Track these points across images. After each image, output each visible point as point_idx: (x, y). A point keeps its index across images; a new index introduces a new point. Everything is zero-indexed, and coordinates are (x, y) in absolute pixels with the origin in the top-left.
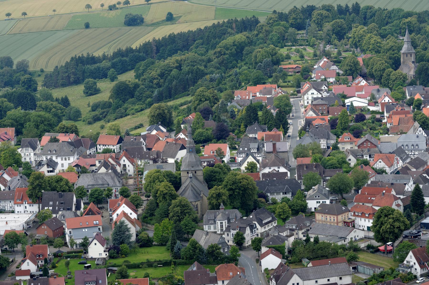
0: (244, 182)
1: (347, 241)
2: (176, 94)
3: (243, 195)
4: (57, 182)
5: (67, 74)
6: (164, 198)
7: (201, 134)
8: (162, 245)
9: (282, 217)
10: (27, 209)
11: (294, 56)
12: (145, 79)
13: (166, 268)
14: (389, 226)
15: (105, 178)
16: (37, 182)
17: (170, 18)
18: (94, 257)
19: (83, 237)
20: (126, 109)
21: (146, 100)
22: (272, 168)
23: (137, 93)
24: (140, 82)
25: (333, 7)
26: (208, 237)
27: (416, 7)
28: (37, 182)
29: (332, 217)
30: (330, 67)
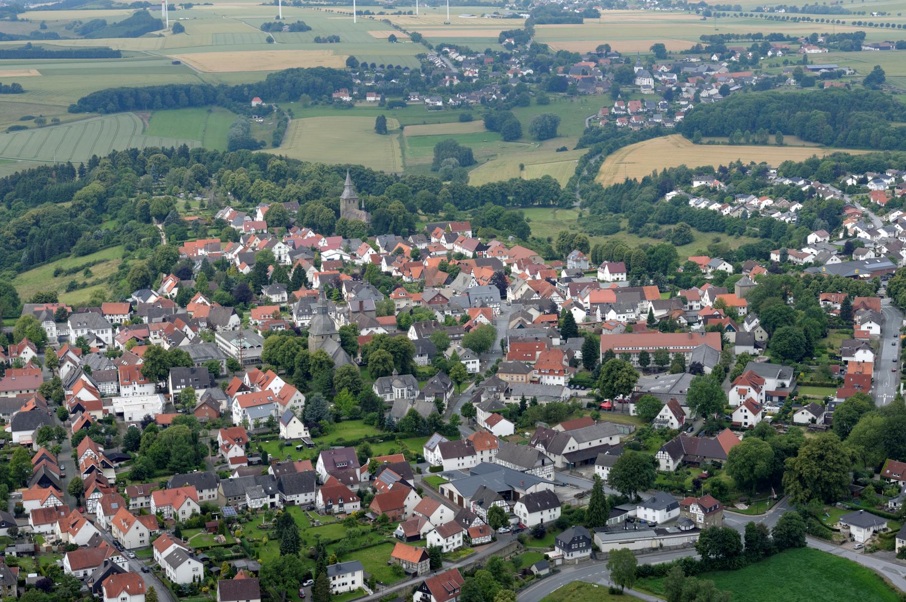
2: (51, 256)
4: (176, 355)
6: (321, 366)
8: (351, 419)
10: (137, 390)
14: (624, 380)
22: (370, 330)
29: (520, 377)
30: (243, 217)
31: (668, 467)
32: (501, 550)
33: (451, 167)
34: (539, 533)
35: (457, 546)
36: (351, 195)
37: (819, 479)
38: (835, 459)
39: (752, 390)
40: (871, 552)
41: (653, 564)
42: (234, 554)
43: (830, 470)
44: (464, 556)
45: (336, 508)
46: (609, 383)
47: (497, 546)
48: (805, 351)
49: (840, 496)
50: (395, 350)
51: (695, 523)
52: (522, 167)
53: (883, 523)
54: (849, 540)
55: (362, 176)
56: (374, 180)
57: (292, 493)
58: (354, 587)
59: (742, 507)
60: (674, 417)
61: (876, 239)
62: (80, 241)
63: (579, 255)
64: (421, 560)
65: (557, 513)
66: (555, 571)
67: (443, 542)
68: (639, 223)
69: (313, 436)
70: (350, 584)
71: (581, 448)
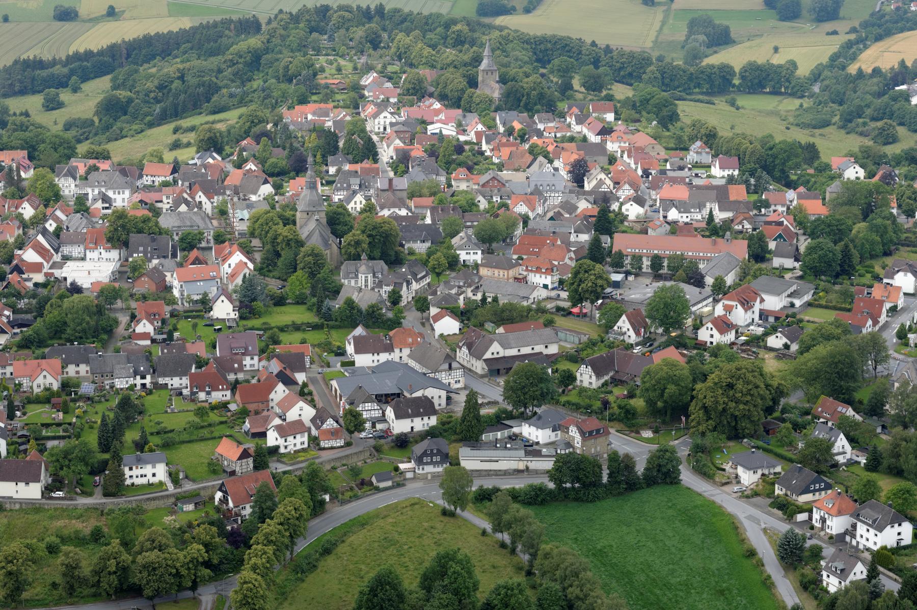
0: (386, 227)
1: (531, 301)
3: (384, 243)
4: (144, 222)
5: (10, 82)
6: (288, 244)
7: (275, 165)
8: (297, 303)
9: (437, 270)
10: (103, 256)
11: (330, 70)
12: (138, 92)
13: (316, 332)
14: (590, 284)
15: (194, 218)
16: (121, 222)
17: (112, 13)
18: (220, 317)
19: (203, 292)
20: (121, 130)
21: (144, 118)
22: (392, 210)
23: (131, 110)
24: (134, 96)
25: (352, 8)
26: (361, 294)
27: (423, 6)
28: (121, 222)
29: (501, 272)
30: (383, 84)
31: (591, 383)
32: (347, 456)
33: (698, 45)
34: (403, 442)
35: (299, 447)
36: (489, 65)
37: (724, 410)
38: (744, 390)
39: (739, 306)
40: (747, 497)
41: (517, 487)
42: (61, 434)
43: (737, 402)
44: (303, 459)
45: (202, 396)
46: (575, 286)
47: (349, 451)
48: (839, 268)
49: (747, 431)
50: (374, 233)
51: (573, 447)
52: (776, 50)
53: (774, 467)
54: (734, 481)
55: (567, 48)
56: (580, 53)
57: (164, 375)
58: (153, 480)
59: (647, 434)
60: (631, 329)
61: (891, 150)
62: (215, 98)
63: (701, 147)
64: (240, 458)
65: (433, 421)
66: (398, 485)
67: (281, 442)
68: (848, 117)
69: (242, 317)
70: (149, 476)
71: (507, 355)
